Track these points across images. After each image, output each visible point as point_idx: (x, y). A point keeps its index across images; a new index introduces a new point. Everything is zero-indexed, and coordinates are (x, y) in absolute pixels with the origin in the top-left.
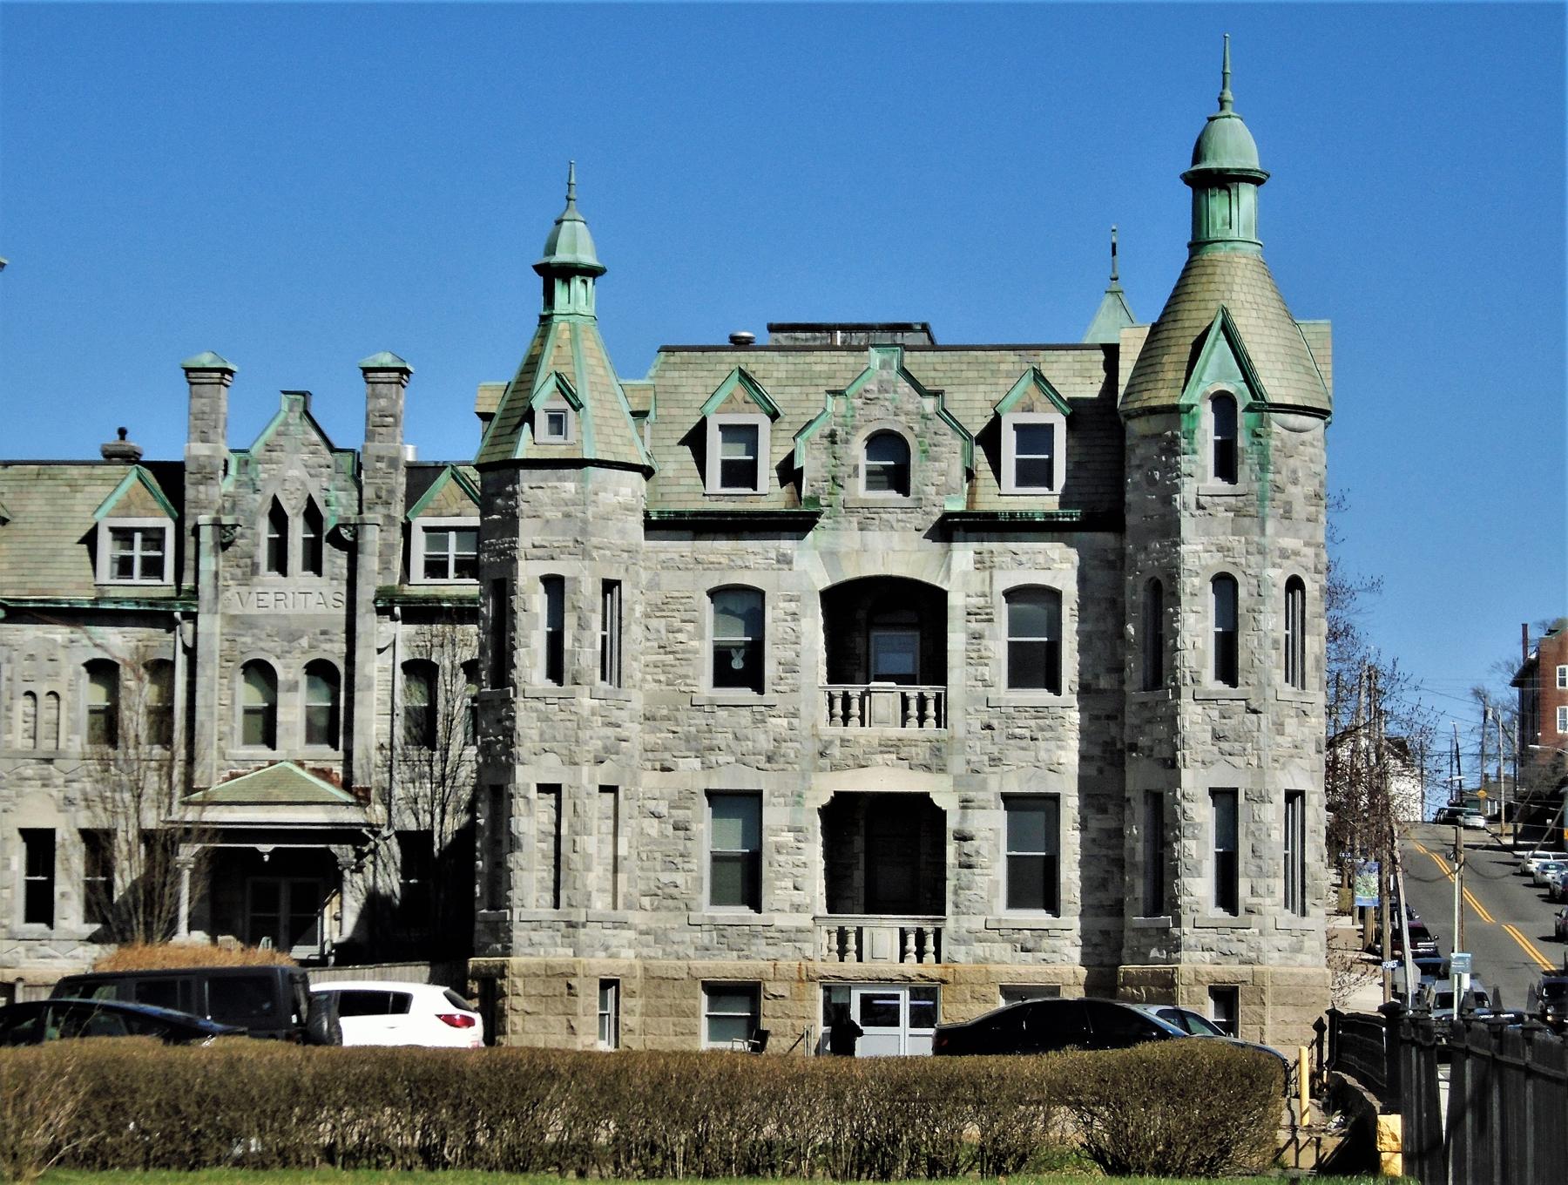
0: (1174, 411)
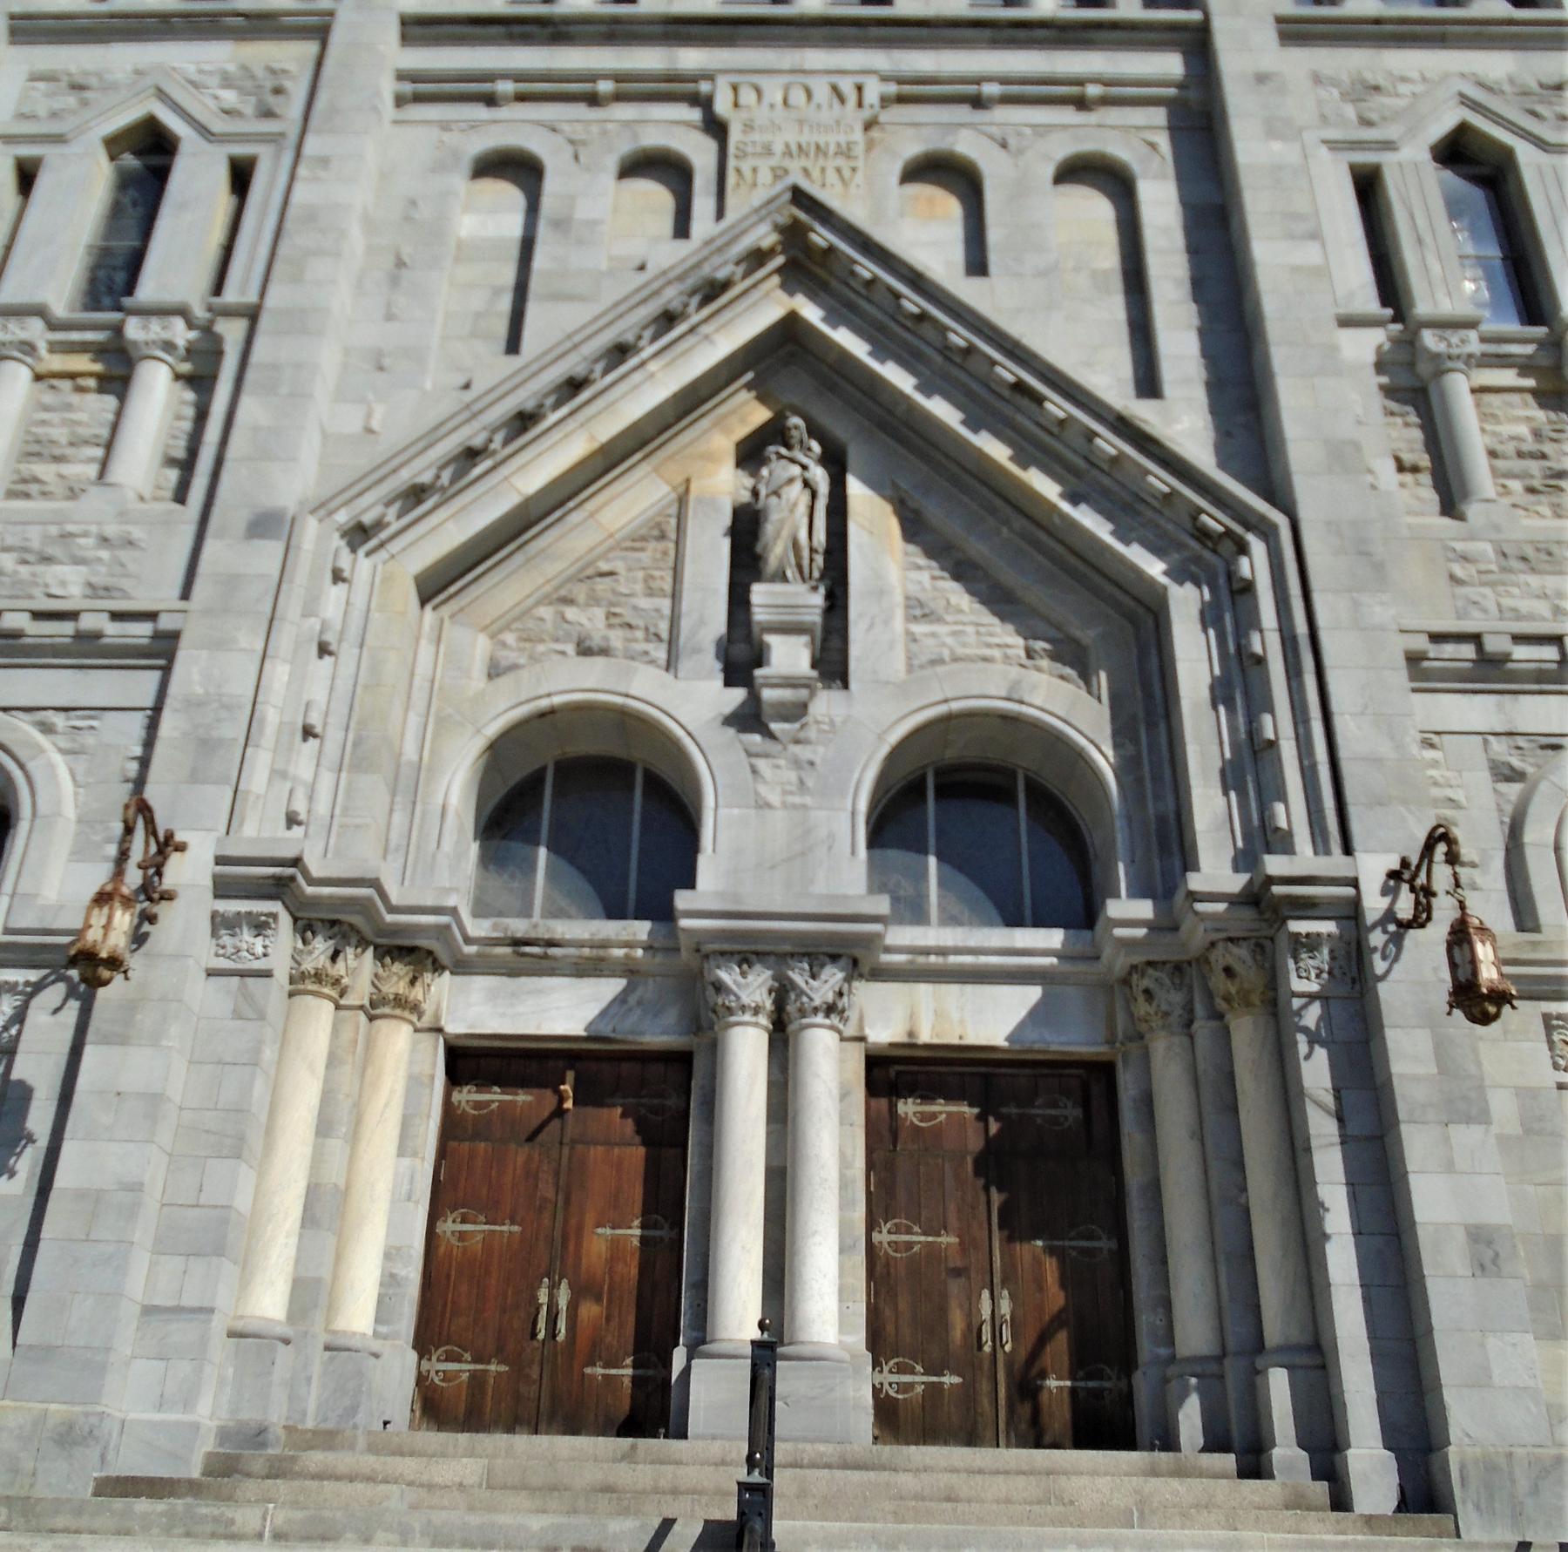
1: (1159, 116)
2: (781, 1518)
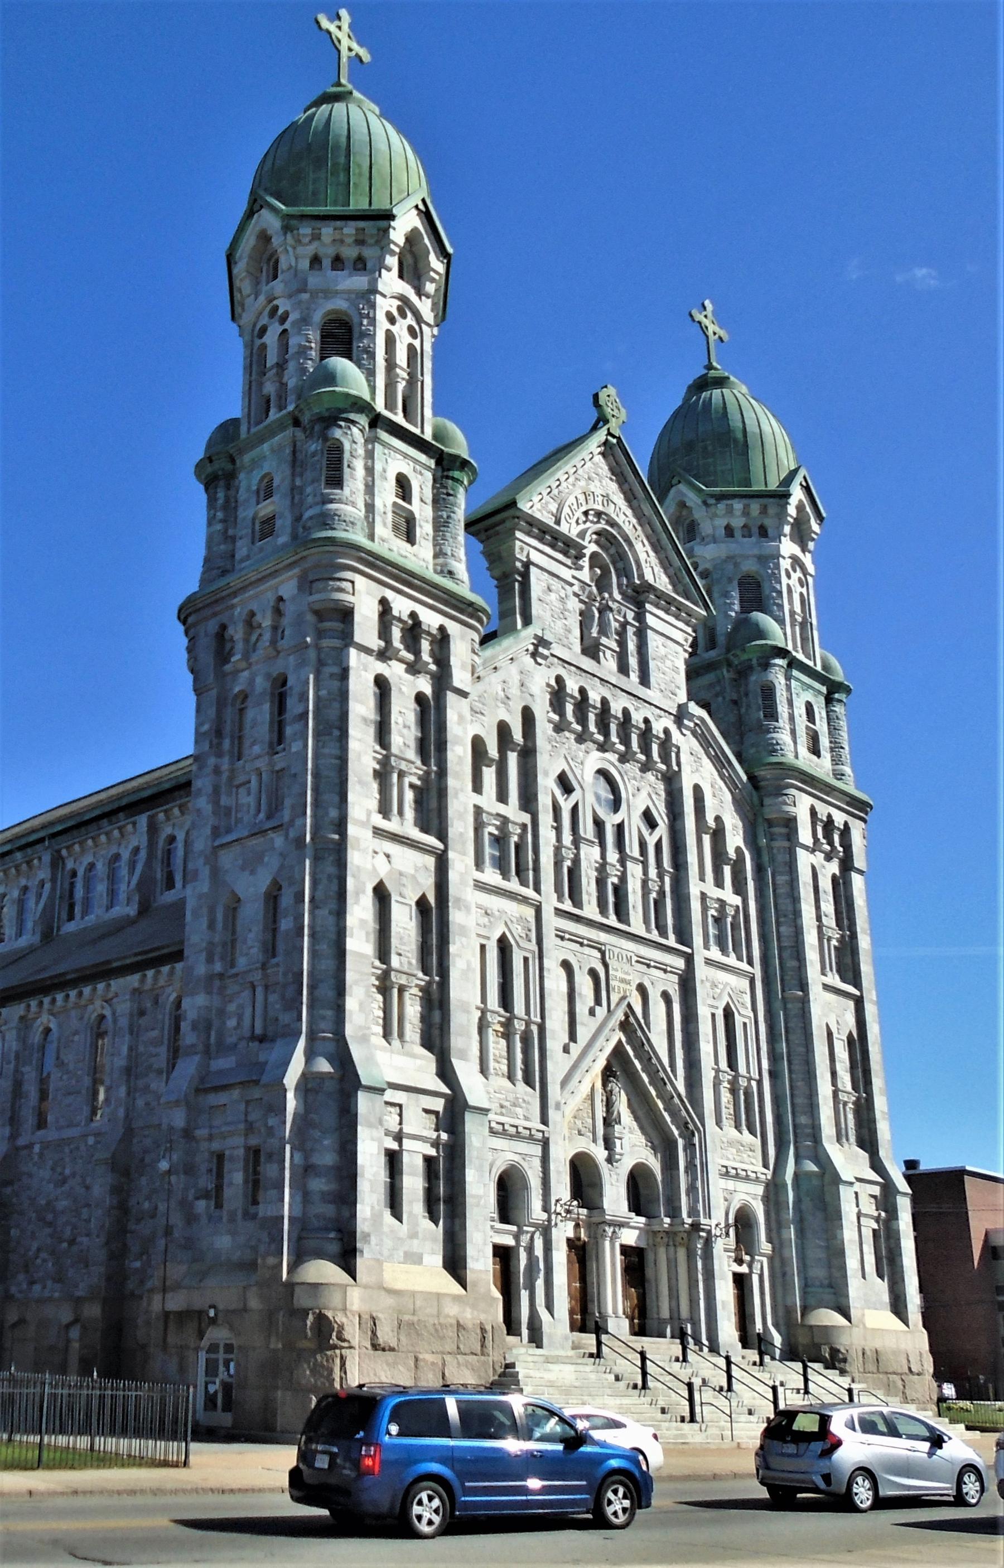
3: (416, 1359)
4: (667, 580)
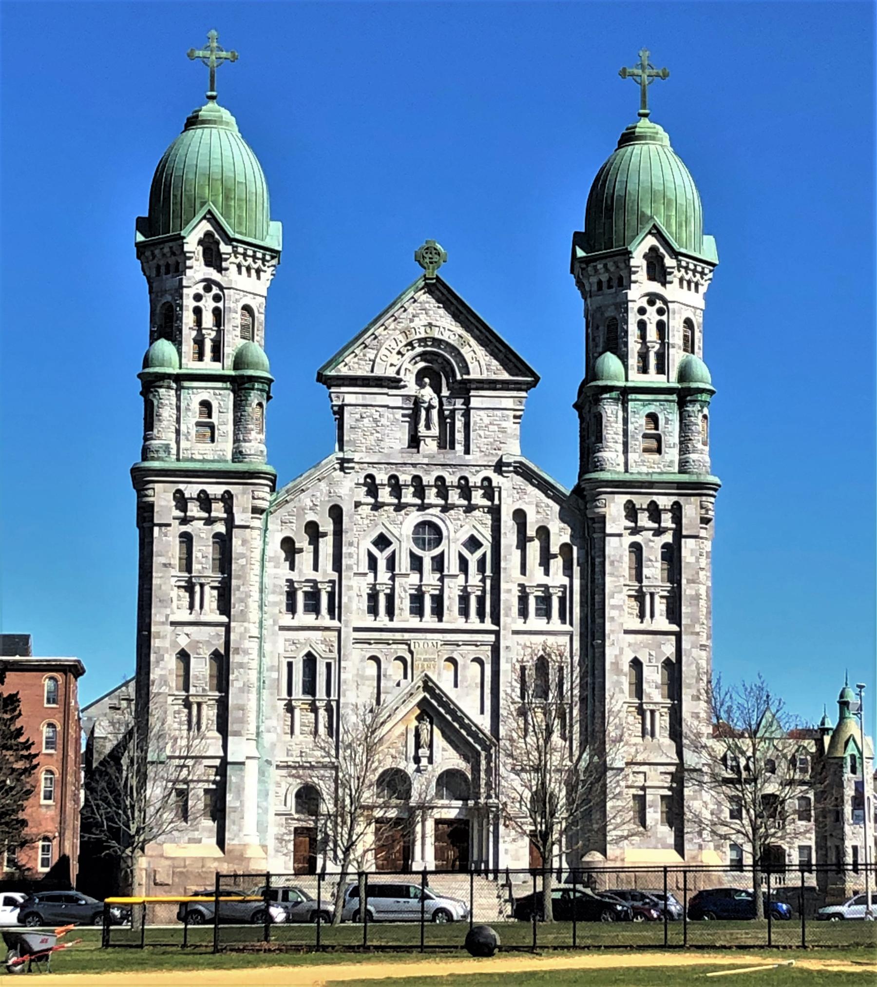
0: (843, 758)
1: (490, 647)
2: (156, 572)
3: (185, 889)
4: (497, 363)
